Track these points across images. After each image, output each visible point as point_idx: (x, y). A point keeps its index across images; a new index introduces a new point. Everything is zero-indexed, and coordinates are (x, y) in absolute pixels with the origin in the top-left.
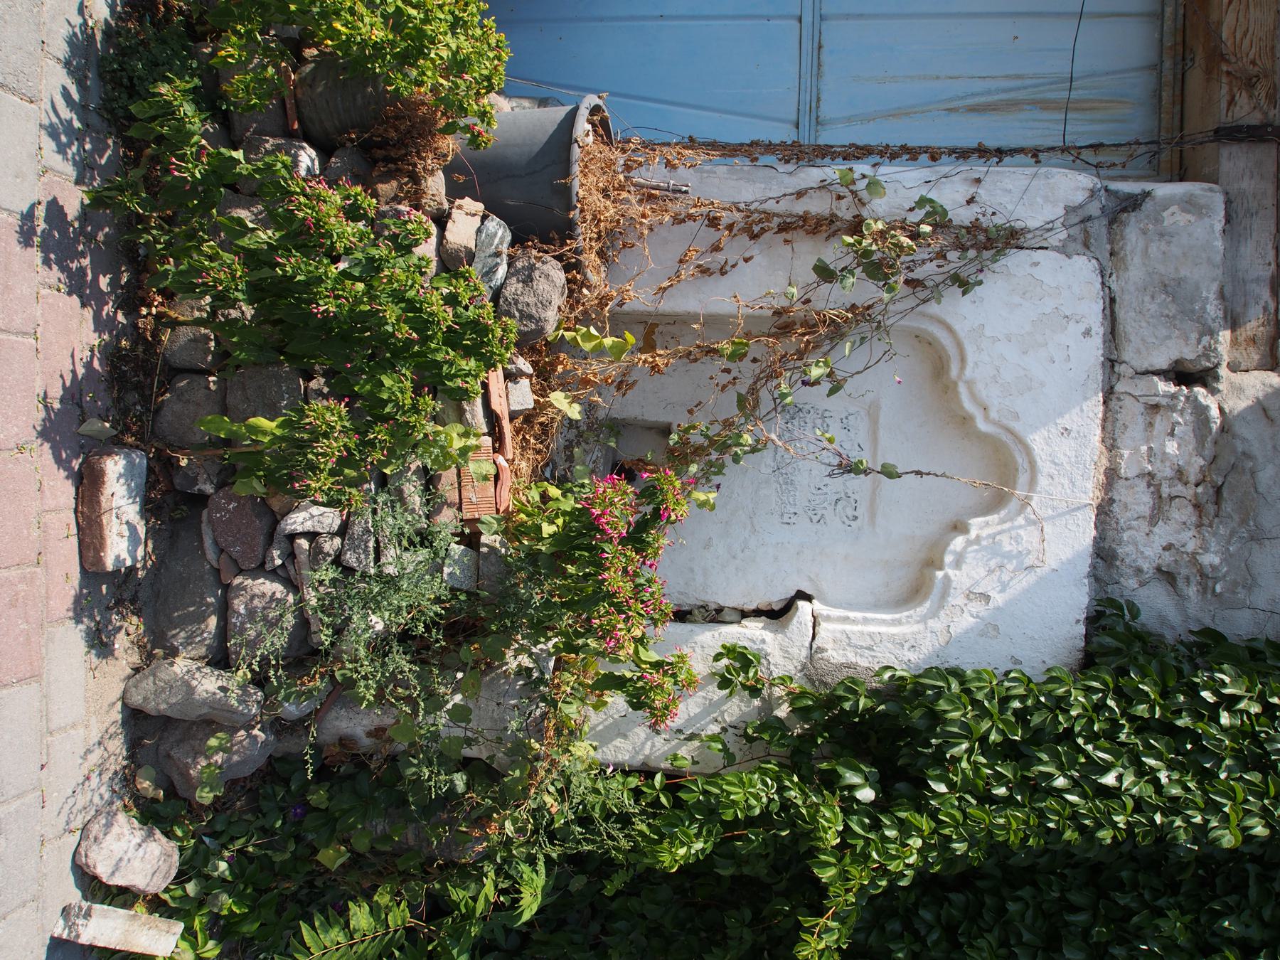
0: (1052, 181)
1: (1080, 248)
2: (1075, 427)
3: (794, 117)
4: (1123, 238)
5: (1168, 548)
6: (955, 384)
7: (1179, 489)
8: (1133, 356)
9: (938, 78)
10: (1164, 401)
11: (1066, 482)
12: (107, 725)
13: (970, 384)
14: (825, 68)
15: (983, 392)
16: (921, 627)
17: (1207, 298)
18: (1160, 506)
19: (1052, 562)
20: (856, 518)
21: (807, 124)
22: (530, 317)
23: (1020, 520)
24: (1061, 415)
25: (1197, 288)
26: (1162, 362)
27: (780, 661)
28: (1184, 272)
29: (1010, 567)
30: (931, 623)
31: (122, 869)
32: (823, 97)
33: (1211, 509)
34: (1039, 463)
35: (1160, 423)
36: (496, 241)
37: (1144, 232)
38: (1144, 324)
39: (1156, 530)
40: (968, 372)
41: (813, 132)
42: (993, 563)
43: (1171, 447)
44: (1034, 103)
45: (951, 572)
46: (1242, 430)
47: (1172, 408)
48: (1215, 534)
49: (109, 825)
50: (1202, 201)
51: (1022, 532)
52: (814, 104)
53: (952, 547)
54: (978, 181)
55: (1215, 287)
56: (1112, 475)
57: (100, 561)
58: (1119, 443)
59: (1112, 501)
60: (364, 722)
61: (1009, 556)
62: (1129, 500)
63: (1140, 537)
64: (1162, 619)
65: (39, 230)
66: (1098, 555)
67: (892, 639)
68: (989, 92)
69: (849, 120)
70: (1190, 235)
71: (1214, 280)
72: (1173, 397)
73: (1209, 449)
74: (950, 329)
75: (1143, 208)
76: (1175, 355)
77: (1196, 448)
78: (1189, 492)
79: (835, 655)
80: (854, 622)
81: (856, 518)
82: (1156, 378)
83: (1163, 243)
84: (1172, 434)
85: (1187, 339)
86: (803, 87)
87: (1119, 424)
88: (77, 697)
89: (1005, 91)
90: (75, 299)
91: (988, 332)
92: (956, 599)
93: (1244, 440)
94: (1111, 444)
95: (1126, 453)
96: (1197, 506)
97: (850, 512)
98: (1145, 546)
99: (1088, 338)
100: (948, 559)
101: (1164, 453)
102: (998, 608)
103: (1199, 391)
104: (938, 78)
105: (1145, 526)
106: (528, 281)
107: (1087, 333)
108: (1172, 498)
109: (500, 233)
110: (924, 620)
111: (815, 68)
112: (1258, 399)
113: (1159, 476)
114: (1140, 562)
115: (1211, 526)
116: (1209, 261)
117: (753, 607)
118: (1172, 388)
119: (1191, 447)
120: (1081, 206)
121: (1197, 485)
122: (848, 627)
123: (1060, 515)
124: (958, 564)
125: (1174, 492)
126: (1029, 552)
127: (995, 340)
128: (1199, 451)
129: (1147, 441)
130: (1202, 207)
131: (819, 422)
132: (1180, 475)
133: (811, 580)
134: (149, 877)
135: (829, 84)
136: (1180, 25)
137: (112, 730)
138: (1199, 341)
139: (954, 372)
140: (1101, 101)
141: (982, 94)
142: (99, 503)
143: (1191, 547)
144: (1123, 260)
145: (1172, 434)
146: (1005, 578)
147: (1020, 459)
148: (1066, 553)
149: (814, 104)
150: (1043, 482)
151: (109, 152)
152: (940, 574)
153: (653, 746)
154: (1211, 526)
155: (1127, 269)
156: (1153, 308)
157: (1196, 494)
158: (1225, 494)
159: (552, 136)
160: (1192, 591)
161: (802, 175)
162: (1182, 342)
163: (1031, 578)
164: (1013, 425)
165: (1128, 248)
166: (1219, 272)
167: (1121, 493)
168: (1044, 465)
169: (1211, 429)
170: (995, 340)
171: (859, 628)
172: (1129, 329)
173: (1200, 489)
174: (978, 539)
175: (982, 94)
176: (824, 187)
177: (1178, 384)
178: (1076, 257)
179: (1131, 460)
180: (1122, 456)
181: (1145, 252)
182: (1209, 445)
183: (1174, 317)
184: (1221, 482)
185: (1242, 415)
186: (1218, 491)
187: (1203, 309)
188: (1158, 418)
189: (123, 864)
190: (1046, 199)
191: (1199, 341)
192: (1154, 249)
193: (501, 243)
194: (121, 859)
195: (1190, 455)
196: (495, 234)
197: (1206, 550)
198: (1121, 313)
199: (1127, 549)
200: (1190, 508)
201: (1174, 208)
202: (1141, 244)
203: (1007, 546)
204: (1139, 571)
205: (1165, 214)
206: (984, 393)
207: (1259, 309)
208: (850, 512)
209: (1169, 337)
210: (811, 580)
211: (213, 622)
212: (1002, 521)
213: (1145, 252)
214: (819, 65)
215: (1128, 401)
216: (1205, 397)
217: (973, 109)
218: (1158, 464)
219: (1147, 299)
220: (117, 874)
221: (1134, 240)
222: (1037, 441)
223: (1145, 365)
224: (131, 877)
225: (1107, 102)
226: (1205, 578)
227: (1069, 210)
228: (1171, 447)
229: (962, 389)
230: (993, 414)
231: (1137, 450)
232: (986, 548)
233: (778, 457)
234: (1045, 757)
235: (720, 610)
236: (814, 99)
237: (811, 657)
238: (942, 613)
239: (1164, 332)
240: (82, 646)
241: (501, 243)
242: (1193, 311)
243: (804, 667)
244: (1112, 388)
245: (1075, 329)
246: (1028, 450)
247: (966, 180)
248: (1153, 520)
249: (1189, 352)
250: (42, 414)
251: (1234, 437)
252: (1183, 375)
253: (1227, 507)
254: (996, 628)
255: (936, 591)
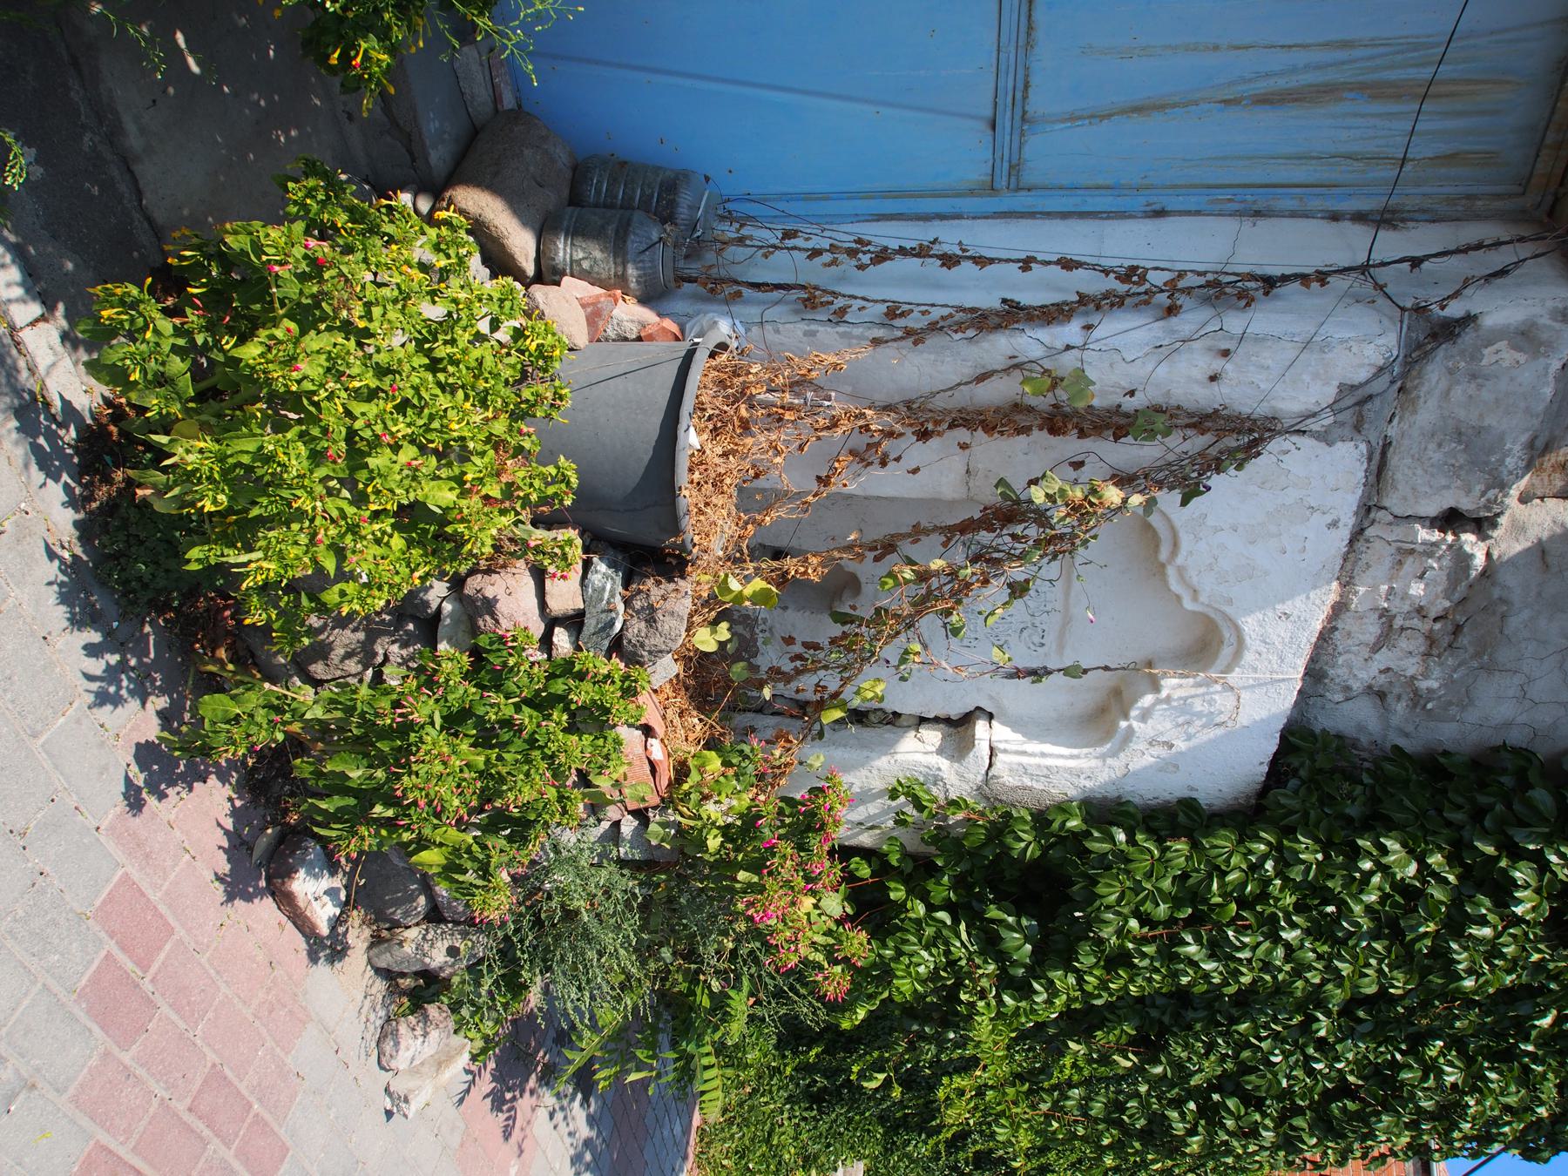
0: (1330, 355)
1: (1347, 431)
2: (1296, 613)
3: (989, 113)
4: (1420, 376)
7: (1416, 622)
9: (1216, 48)
10: (1420, 549)
13: (1181, 571)
14: (1039, 34)
15: (1192, 575)
16: (1099, 763)
17: (1510, 450)
18: (1385, 639)
19: (1243, 720)
20: (1043, 645)
21: (1008, 125)
24: (1283, 601)
25: (1501, 438)
26: (1432, 508)
27: (957, 783)
28: (1490, 421)
29: (1198, 723)
30: (1109, 761)
32: (1034, 81)
34: (1248, 641)
35: (1410, 565)
36: (606, 595)
37: (1451, 372)
38: (1419, 472)
39: (1377, 656)
40: (1179, 560)
41: (1016, 138)
42: (1181, 720)
44: (1361, 87)
45: (1135, 724)
46: (1509, 579)
47: (1430, 555)
49: (397, 1044)
50: (1545, 336)
51: (1216, 697)
52: (1019, 95)
53: (1139, 704)
54: (1226, 353)
55: (1524, 438)
59: (1335, 629)
61: (1199, 715)
62: (1355, 629)
63: (1357, 661)
64: (1361, 728)
65: (141, 784)
67: (1070, 771)
68: (1294, 70)
69: (1073, 118)
70: (1512, 379)
71: (1527, 430)
72: (1435, 544)
73: (1462, 588)
75: (1459, 341)
77: (1446, 590)
78: (1425, 626)
79: (1009, 780)
80: (1032, 755)
81: (1043, 645)
82: (1417, 526)
83: (1473, 386)
86: (1003, 67)
89: (1319, 67)
91: (1210, 522)
92: (1138, 745)
95: (1362, 590)
97: (1037, 640)
98: (1358, 668)
99: (1333, 530)
100: (1134, 713)
102: (1181, 753)
103: (1468, 538)
104: (1216, 48)
105: (1365, 653)
106: (651, 621)
107: (1334, 524)
109: (608, 587)
110: (1103, 757)
111: (1023, 36)
112: (1540, 540)
114: (1351, 682)
115: (1439, 656)
116: (1527, 410)
117: (931, 716)
118: (1436, 536)
119: (1440, 589)
120: (1361, 385)
121: (1435, 620)
122: (1025, 760)
124: (1145, 716)
125: (1407, 624)
127: (1217, 529)
128: (1448, 593)
129: (1391, 579)
130: (1541, 344)
133: (991, 698)
135: (1045, 57)
138: (1483, 494)
139: (1164, 555)
140: (1469, 82)
141: (1281, 73)
143: (1411, 672)
144: (1414, 402)
146: (1191, 730)
147: (1227, 634)
149: (1019, 95)
150: (1249, 657)
151: (152, 638)
152: (1123, 724)
155: (1415, 412)
156: (1437, 456)
157: (1431, 630)
159: (648, 468)
160: (1400, 707)
161: (985, 345)
162: (1462, 493)
163: (1220, 731)
165: (1424, 389)
168: (1252, 641)
170: (1217, 529)
171: (1037, 760)
172: (1399, 476)
173: (1438, 626)
174: (1168, 699)
175: (1281, 73)
176: (1016, 366)
177: (1443, 530)
178: (1339, 444)
179: (1369, 592)
180: (1356, 593)
181: (1446, 394)
183: (1461, 467)
184: (1470, 617)
185: (1513, 562)
187: (1501, 462)
190: (1316, 376)
191: (1483, 494)
192: (1458, 393)
193: (612, 595)
195: (1437, 596)
196: (604, 589)
199: (1339, 672)
200: (1421, 640)
201: (1502, 345)
202: (1444, 384)
203: (1198, 706)
204: (1348, 688)
205: (1486, 352)
206: (1195, 580)
208: (1037, 640)
209: (1448, 487)
210: (991, 698)
211: (422, 900)
212: (1199, 685)
213: (1446, 394)
214: (1030, 28)
215: (1378, 544)
216: (1473, 544)
217: (1266, 100)
218: (1397, 602)
219: (1432, 446)
221: (1434, 381)
225: (1477, 82)
226: (1417, 699)
227: (1346, 389)
229: (1171, 572)
231: (1375, 588)
232: (1175, 708)
234: (1189, 938)
235: (896, 714)
236: (1020, 86)
237: (986, 781)
238: (1122, 755)
239: (1444, 482)
241: (612, 595)
242: (1486, 463)
243: (979, 788)
244: (1363, 530)
245: (1320, 520)
246: (1238, 630)
247: (1210, 349)
248: (1376, 648)
250: (222, 888)
252: (1451, 520)
253: (1464, 640)
254: (1177, 767)
255: (1118, 737)
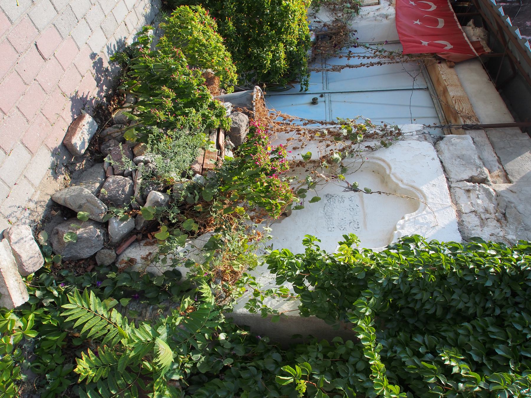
5: (492, 235)
6: (389, 175)
7: (488, 216)
8: (453, 176)
11: (439, 200)
12: (42, 199)
18: (483, 223)
22: (236, 123)
23: (424, 212)
28: (464, 153)
31: (20, 243)
33: (503, 221)
40: (393, 170)
43: (479, 202)
47: (475, 190)
48: (510, 228)
51: (426, 216)
56: (459, 213)
57: (71, 138)
58: (459, 202)
60: (142, 254)
62: (470, 220)
66: (464, 239)
71: (475, 154)
72: (474, 186)
74: (384, 161)
76: (470, 175)
84: (478, 198)
85: (472, 170)
87: (457, 197)
88: (36, 182)
90: (96, 83)
93: (506, 197)
94: (456, 203)
95: (463, 205)
96: (498, 221)
97: (356, 226)
101: (478, 204)
105: (479, 229)
108: (487, 219)
113: (478, 212)
123: (440, 210)
126: (431, 222)
131: (340, 200)
132: (487, 211)
134: (28, 258)
136: (444, 118)
137: (43, 204)
138: (477, 170)
139: (388, 172)
142: (78, 124)
143: (501, 234)
144: (442, 151)
145: (478, 198)
147: (419, 195)
148: (446, 222)
152: (396, 232)
153: (271, 303)
154: (506, 226)
157: (496, 216)
158: (507, 215)
164: (413, 184)
165: (442, 149)
166: (476, 152)
167: (465, 218)
169: (492, 196)
173: (497, 214)
182: (494, 200)
186: (504, 214)
188: (471, 194)
189: (22, 241)
194: (22, 239)
197: (509, 234)
198: (446, 165)
200: (496, 222)
207: (497, 168)
208: (356, 226)
219: (454, 160)
220: (17, 244)
222: (424, 189)
223: (460, 178)
224: (22, 251)
228: (479, 202)
229: (391, 176)
230: (405, 181)
231: (466, 204)
233: (325, 211)
240: (48, 165)
242: (471, 162)
249: (475, 173)
251: (502, 197)
